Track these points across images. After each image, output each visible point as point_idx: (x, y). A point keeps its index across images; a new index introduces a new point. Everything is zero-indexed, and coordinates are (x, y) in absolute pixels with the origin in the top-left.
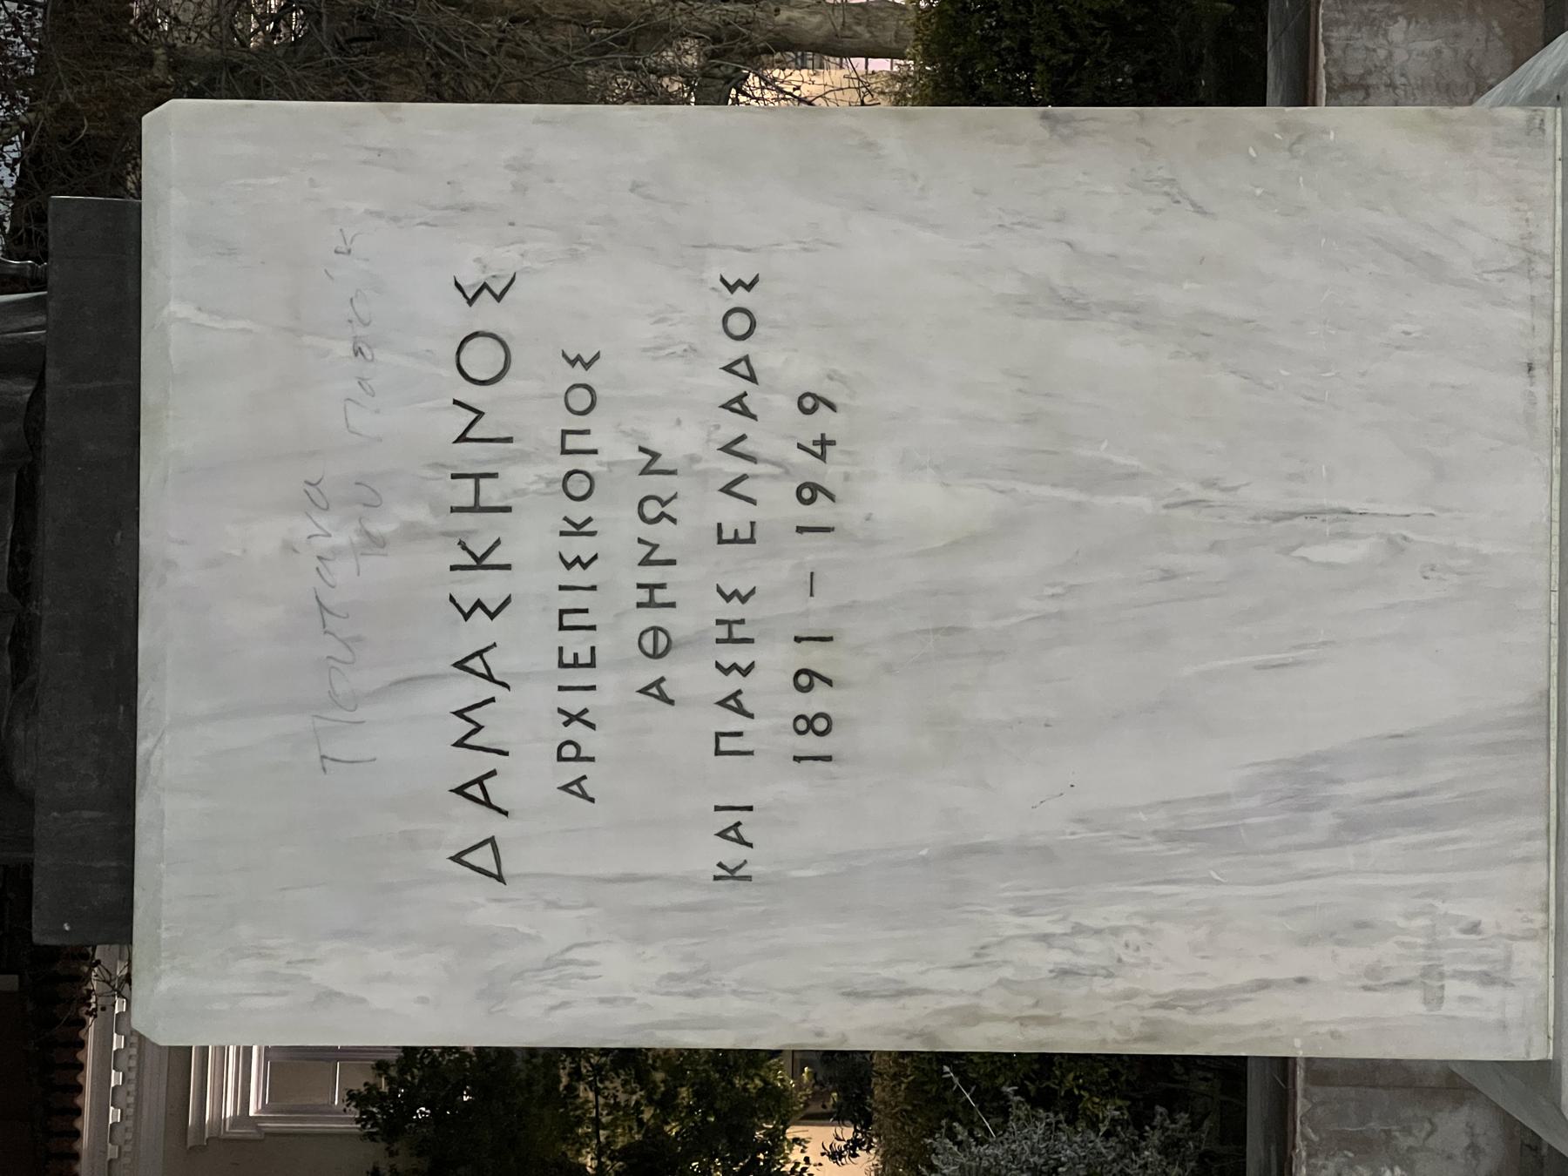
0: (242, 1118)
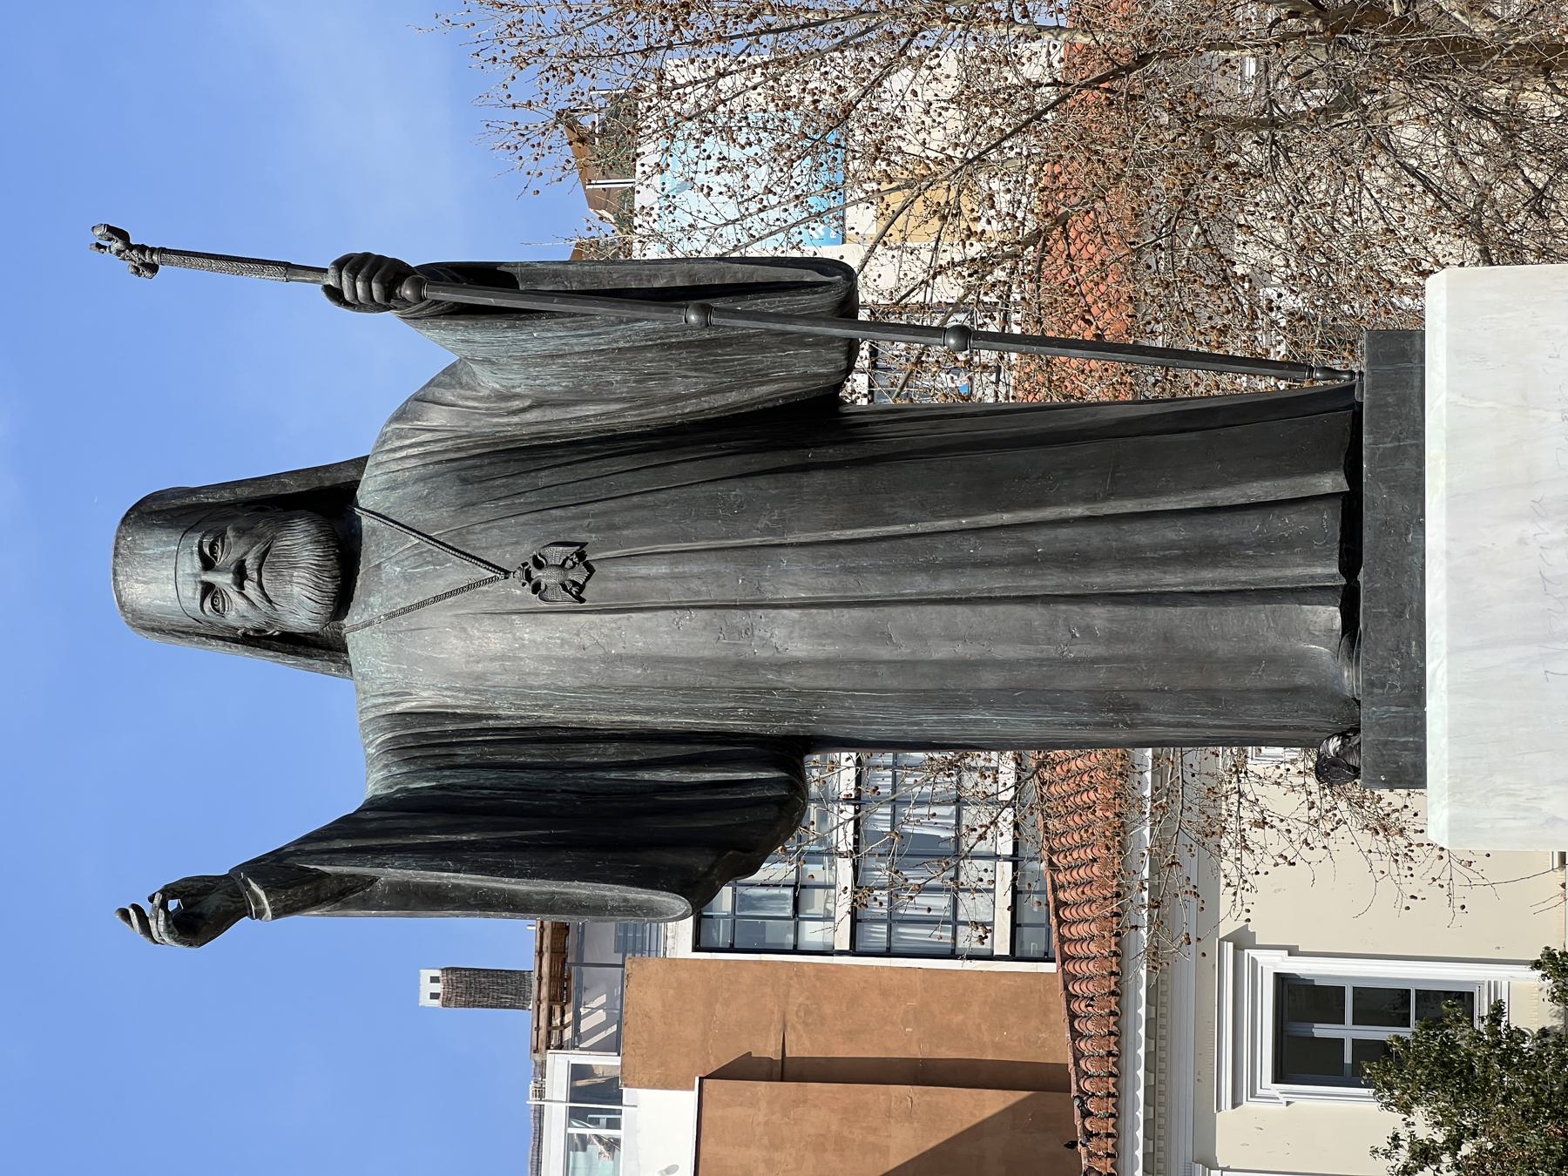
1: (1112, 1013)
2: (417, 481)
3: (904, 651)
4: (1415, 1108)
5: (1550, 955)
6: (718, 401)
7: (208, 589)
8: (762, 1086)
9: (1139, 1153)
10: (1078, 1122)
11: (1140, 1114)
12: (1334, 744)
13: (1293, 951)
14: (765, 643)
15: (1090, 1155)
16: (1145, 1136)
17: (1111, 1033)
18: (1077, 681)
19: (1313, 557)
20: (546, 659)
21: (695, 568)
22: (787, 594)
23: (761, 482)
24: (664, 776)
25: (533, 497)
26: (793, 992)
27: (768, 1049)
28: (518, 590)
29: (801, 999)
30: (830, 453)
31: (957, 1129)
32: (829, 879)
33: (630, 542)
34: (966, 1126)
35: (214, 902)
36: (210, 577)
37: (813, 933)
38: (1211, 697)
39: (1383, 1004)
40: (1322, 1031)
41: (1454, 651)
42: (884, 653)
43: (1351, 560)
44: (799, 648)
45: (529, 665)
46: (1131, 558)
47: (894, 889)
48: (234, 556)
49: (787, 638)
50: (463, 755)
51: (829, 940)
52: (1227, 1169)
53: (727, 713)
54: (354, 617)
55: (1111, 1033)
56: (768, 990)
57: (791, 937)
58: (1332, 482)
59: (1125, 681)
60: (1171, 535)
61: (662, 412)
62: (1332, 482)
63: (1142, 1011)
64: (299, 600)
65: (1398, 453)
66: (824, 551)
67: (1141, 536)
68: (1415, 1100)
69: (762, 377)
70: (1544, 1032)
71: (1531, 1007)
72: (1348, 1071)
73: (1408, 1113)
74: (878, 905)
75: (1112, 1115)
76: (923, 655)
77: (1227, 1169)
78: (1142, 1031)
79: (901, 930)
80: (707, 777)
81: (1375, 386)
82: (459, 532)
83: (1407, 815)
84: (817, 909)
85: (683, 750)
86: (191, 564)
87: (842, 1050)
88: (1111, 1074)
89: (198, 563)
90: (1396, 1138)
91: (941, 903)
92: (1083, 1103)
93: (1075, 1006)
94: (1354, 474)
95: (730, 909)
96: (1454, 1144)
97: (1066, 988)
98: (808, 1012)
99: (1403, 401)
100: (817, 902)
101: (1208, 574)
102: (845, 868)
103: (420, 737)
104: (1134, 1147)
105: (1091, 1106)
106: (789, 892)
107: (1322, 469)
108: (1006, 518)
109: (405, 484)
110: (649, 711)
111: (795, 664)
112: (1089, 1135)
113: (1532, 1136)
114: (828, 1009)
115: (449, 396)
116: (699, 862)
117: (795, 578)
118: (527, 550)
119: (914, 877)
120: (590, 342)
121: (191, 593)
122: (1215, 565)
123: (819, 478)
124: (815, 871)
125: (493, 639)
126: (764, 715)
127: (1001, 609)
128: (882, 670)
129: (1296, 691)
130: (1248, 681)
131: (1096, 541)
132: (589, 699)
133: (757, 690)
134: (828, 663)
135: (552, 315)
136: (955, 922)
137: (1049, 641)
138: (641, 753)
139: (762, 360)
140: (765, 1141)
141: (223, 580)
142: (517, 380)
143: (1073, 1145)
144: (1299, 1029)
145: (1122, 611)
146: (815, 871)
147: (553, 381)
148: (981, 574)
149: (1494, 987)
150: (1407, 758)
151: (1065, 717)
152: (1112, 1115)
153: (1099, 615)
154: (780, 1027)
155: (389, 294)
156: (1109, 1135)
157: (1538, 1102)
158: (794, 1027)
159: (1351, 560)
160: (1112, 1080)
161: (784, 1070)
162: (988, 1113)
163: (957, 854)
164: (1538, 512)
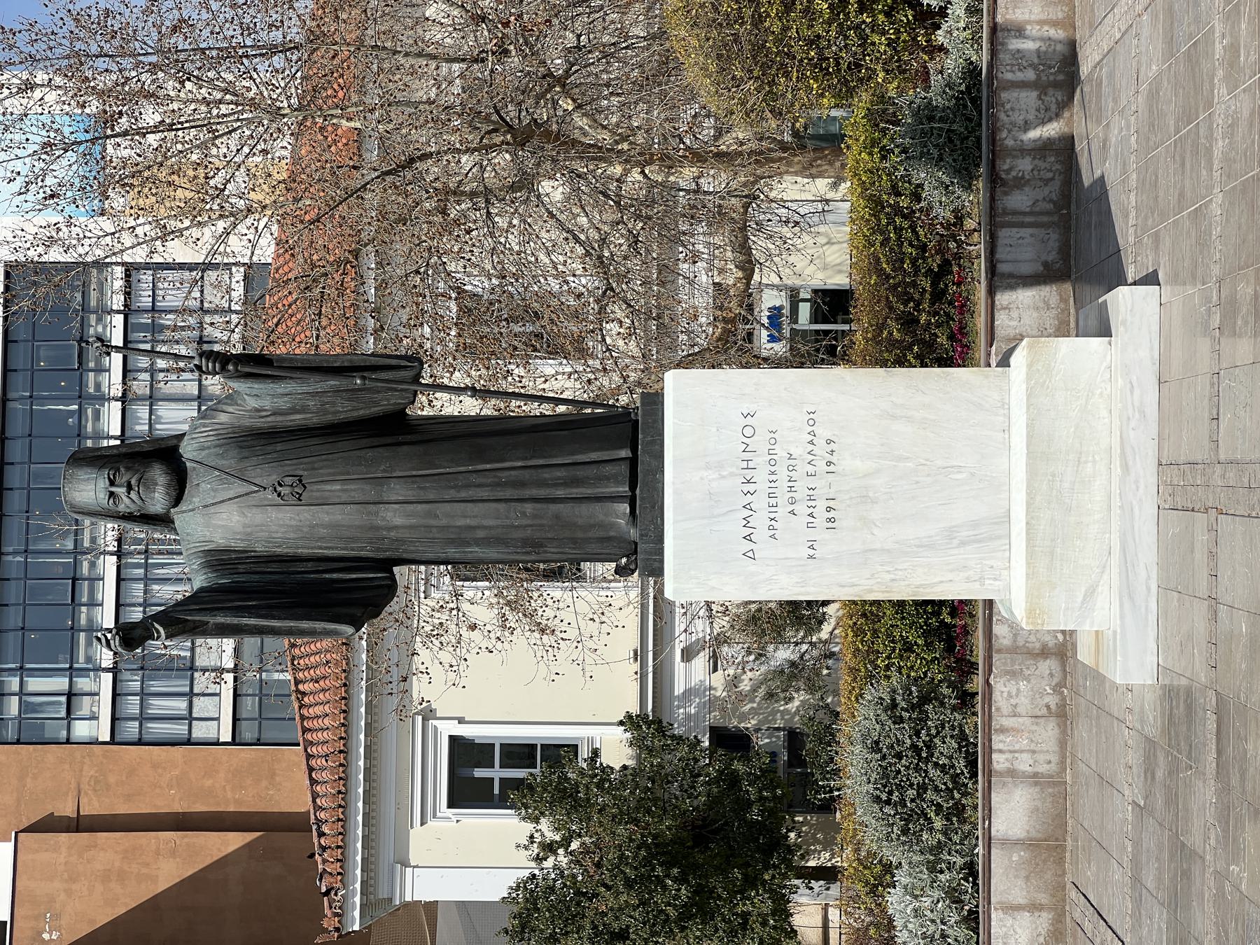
1: (341, 765)
2: (216, 446)
3: (444, 522)
4: (543, 820)
5: (629, 716)
6: (355, 414)
7: (112, 494)
8: (63, 836)
9: (359, 858)
10: (315, 840)
11: (360, 832)
12: (624, 560)
13: (461, 721)
14: (384, 519)
15: (325, 861)
16: (363, 847)
17: (340, 778)
18: (519, 534)
19: (618, 483)
20: (281, 526)
21: (353, 487)
22: (394, 498)
23: (380, 450)
24: (335, 576)
25: (275, 455)
26: (86, 767)
27: (67, 809)
28: (270, 496)
29: (92, 773)
30: (409, 438)
31: (208, 861)
32: (94, 688)
33: (322, 475)
34: (215, 859)
35: (138, 632)
36: (113, 489)
37: (82, 730)
38: (574, 541)
39: (519, 753)
40: (479, 773)
41: (675, 522)
42: (433, 522)
43: (633, 487)
44: (398, 521)
45: (274, 528)
46: (543, 484)
47: (144, 694)
48: (125, 479)
49: (394, 517)
50: (241, 568)
51: (94, 734)
52: (417, 867)
53: (362, 549)
54: (183, 506)
55: (340, 778)
56: (67, 766)
57: (65, 733)
58: (625, 453)
59: (538, 535)
60: (559, 474)
61: (330, 418)
62: (625, 453)
63: (361, 763)
64: (157, 501)
65: (653, 442)
66: (410, 480)
67: (546, 474)
68: (542, 814)
69: (376, 404)
70: (625, 767)
71: (617, 751)
72: (496, 799)
73: (537, 823)
74: (132, 705)
75: (340, 834)
76: (452, 523)
77: (417, 867)
78: (361, 777)
79: (149, 725)
80: (354, 576)
81: (643, 415)
82: (240, 470)
83: (557, 621)
84: (85, 711)
85: (342, 565)
86: (103, 483)
87: (123, 808)
88: (340, 806)
89: (107, 482)
90: (532, 837)
91: (180, 705)
92: (319, 827)
93: (313, 762)
94: (634, 450)
95: (17, 713)
96: (566, 842)
97: (306, 750)
98: (97, 782)
99: (655, 421)
100: (85, 706)
101: (575, 490)
102: (107, 678)
103: (218, 559)
104: (355, 854)
105: (325, 829)
106: (63, 699)
107: (621, 448)
108: (488, 466)
109: (209, 448)
110: (326, 548)
111: (396, 527)
112: (324, 849)
113: (620, 830)
114: (112, 779)
115: (230, 409)
116: (358, 612)
117: (397, 491)
118: (274, 478)
119: (156, 686)
120: (305, 389)
121: (103, 497)
122: (578, 487)
123: (405, 448)
124: (83, 683)
125: (257, 516)
126: (378, 550)
127: (486, 504)
128: (434, 530)
129: (609, 539)
130: (590, 535)
131: (527, 477)
132: (300, 543)
133: (378, 539)
134: (411, 527)
135: (286, 378)
136: (190, 718)
137: (507, 518)
138: (323, 566)
139: (379, 396)
140: (66, 876)
141: (120, 491)
142: (267, 403)
143: (312, 856)
144: (464, 772)
145: (538, 506)
146: (83, 683)
147: (283, 404)
148: (478, 490)
149: (591, 740)
150: (656, 565)
151: (511, 549)
152: (340, 834)
153: (529, 508)
154: (75, 793)
155: (223, 369)
156: (338, 847)
157: (621, 812)
158: (86, 794)
159: (633, 487)
160: (341, 810)
161: (79, 824)
162: (231, 849)
163: (192, 668)
164: (708, 467)
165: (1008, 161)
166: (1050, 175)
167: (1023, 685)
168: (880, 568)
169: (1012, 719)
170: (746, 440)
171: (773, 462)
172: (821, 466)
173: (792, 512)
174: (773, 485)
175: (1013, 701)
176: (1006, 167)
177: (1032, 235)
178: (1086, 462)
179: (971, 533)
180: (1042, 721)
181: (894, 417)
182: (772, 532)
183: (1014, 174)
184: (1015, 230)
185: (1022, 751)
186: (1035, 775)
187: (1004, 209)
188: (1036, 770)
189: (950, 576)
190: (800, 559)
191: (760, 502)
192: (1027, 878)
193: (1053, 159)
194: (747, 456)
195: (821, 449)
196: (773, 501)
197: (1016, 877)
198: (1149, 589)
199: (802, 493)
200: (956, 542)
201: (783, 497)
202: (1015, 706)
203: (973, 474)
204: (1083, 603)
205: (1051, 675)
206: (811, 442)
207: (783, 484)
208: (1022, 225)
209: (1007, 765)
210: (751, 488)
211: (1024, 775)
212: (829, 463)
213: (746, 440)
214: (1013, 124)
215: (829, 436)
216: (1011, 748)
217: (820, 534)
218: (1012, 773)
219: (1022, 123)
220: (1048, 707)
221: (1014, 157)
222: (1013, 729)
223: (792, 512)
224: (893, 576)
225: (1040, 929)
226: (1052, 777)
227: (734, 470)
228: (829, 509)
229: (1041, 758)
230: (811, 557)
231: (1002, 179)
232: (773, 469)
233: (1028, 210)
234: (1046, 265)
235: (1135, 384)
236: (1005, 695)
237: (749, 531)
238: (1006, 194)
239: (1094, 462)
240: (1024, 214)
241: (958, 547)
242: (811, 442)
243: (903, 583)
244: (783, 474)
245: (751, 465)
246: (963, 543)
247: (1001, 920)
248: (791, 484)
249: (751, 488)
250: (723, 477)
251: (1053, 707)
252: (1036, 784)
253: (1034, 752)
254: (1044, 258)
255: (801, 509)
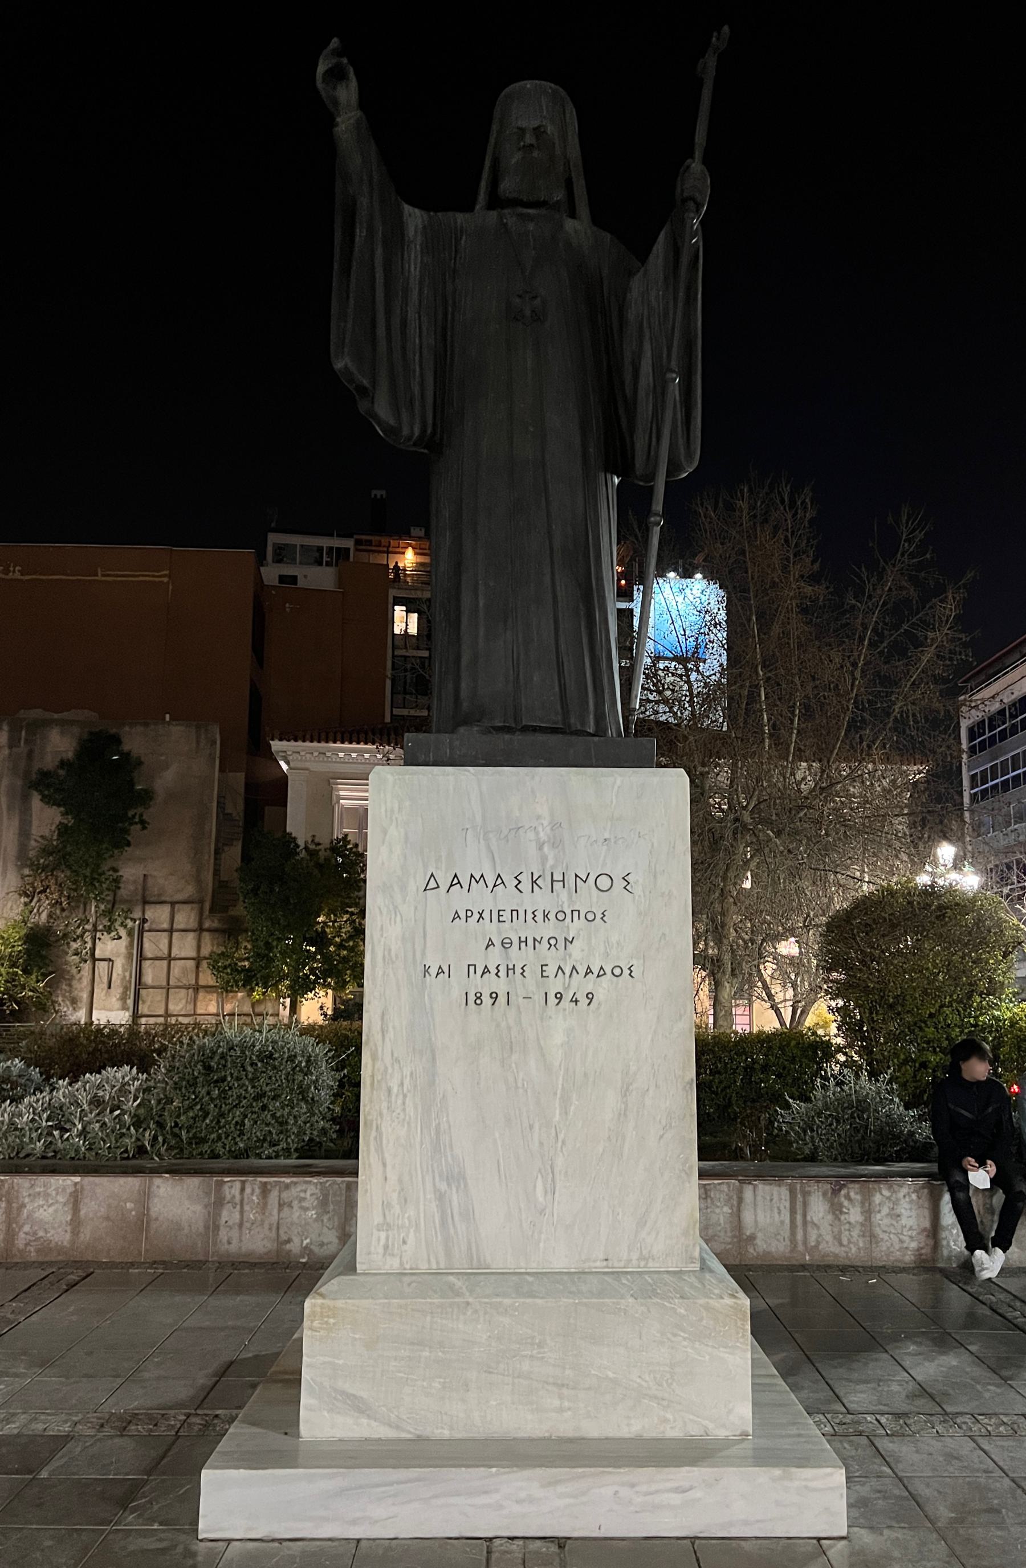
0: (339, 798)
164: (555, 826)
165: (858, 1197)
166: (845, 1242)
167: (312, 1213)
168: (407, 1072)
169: (276, 1202)
170: (591, 880)
171: (561, 916)
172: (555, 985)
173: (490, 943)
174: (530, 916)
175: (295, 1203)
176: (852, 1194)
177: (782, 1222)
178: (561, 1397)
179: (456, 1211)
180: (273, 1234)
181: (625, 1092)
182: (463, 915)
183: (846, 1203)
184: (788, 1204)
185: (242, 1212)
186: (217, 1228)
187: (809, 1193)
188: (221, 1228)
189: (392, 1177)
190: (423, 954)
191: (506, 898)
192: (107, 1218)
193: (861, 1245)
194: (570, 880)
195: (580, 985)
196: (506, 916)
197: (109, 1206)
198: (354, 1522)
199: (517, 957)
200: (443, 1186)
201: (512, 931)
202: (290, 1206)
203: (542, 1212)
204: (343, 1393)
205: (322, 1245)
206: (589, 971)
207: (529, 932)
208: (793, 1211)
209: (228, 1197)
210: (526, 885)
211: (217, 1215)
212: (559, 997)
213: (591, 880)
214: (896, 1203)
215: (600, 996)
216: (246, 1200)
217: (457, 985)
218: (219, 1203)
219: (898, 1212)
220: (289, 1241)
221: (863, 1203)
222: (265, 1204)
223: (490, 943)
224: (395, 1090)
225: (52, 1232)
226: (215, 1244)
227: (551, 862)
228: (494, 996)
229: (235, 1233)
230: (426, 970)
231: (840, 1190)
232: (552, 916)
233: (809, 1218)
234: (752, 1238)
235: (690, 1495)
236: (302, 1195)
237: (465, 881)
238: (825, 1194)
239: (561, 1410)
240: (805, 1216)
241: (436, 1190)
242: (589, 971)
243: (385, 1105)
244: (547, 930)
245: (558, 886)
246: (440, 1197)
247: (64, 1190)
248: (530, 942)
249: (526, 885)
250: (540, 848)
251: (288, 1247)
252: (207, 1228)
253: (241, 1225)
254: (760, 1235)
255: (495, 957)
